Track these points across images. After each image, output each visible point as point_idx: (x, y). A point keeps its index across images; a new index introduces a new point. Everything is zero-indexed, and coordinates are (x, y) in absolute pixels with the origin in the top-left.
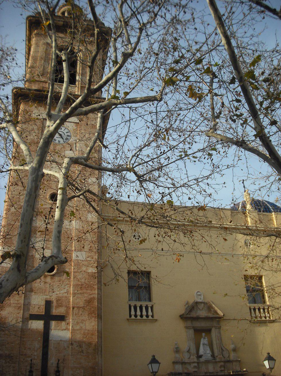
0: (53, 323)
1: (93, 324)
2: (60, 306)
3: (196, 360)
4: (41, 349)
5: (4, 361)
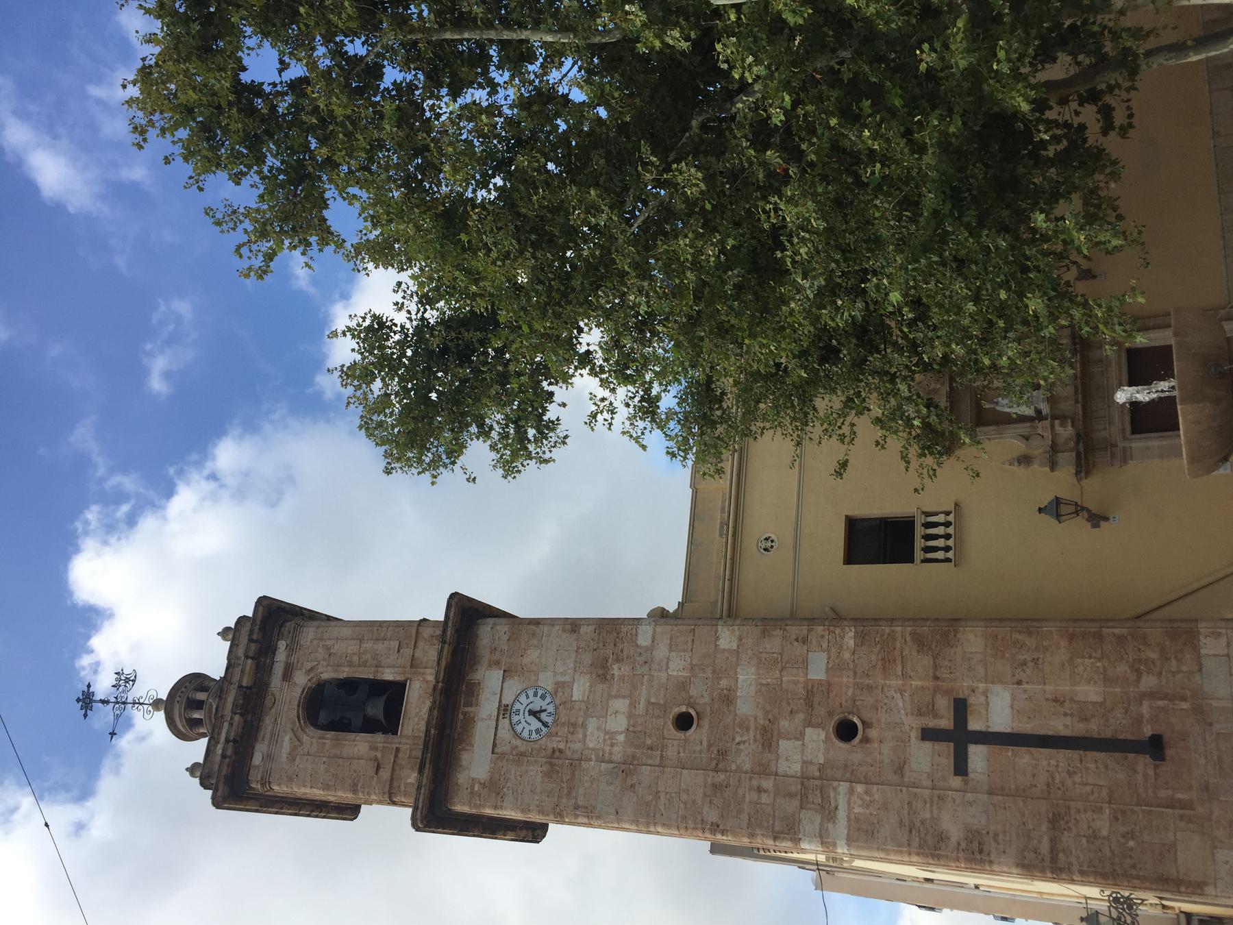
0: (974, 725)
1: (972, 637)
2: (933, 706)
3: (1047, 423)
4: (1032, 750)
5: (1066, 833)
